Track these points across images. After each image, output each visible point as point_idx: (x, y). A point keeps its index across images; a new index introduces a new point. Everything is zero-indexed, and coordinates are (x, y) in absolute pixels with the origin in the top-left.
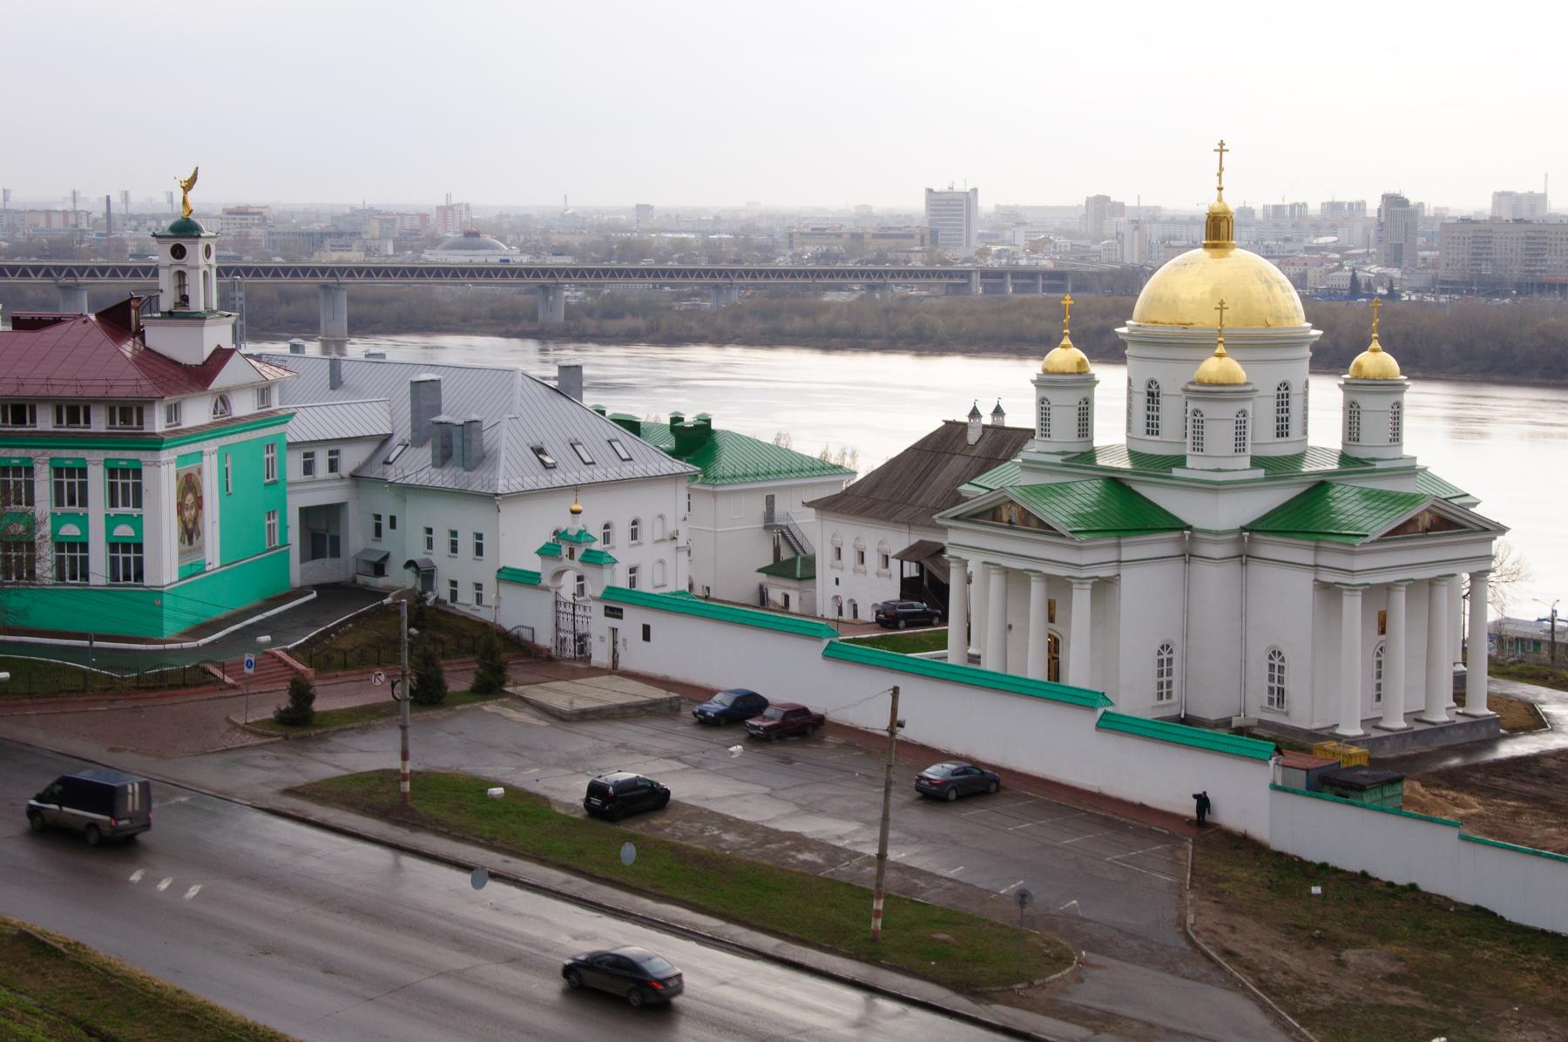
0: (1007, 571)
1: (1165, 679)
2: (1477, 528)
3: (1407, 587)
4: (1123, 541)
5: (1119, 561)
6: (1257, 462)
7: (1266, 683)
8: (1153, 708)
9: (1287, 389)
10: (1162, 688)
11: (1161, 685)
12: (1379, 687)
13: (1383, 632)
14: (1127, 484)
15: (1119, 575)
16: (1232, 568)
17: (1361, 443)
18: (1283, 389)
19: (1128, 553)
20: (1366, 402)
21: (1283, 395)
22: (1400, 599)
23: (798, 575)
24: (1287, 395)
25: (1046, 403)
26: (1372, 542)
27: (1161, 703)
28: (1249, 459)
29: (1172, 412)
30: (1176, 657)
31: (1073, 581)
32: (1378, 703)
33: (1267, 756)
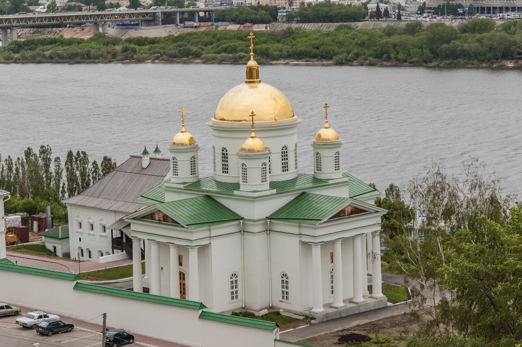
0: (159, 243)
1: (234, 290)
2: (373, 211)
3: (341, 241)
4: (211, 227)
5: (210, 237)
6: (273, 185)
7: (281, 289)
8: (229, 303)
9: (286, 149)
10: (233, 294)
11: (232, 293)
12: (332, 287)
13: (332, 262)
14: (213, 197)
15: (210, 243)
16: (264, 236)
17: (322, 172)
18: (284, 149)
19: (214, 233)
20: (324, 153)
21: (284, 152)
22: (339, 246)
23: (60, 237)
24: (287, 152)
25: (175, 159)
26: (324, 222)
27: (233, 301)
28: (268, 185)
29: (234, 163)
30: (239, 279)
31: (189, 247)
32: (332, 295)
33: (273, 328)
